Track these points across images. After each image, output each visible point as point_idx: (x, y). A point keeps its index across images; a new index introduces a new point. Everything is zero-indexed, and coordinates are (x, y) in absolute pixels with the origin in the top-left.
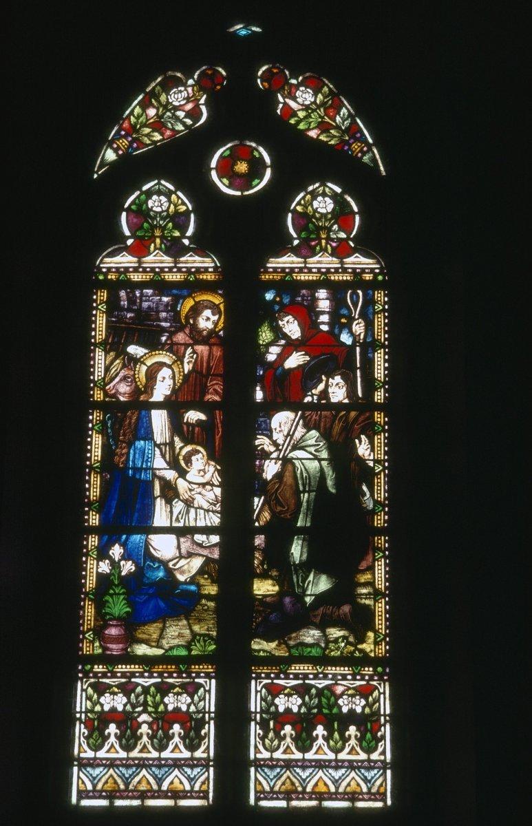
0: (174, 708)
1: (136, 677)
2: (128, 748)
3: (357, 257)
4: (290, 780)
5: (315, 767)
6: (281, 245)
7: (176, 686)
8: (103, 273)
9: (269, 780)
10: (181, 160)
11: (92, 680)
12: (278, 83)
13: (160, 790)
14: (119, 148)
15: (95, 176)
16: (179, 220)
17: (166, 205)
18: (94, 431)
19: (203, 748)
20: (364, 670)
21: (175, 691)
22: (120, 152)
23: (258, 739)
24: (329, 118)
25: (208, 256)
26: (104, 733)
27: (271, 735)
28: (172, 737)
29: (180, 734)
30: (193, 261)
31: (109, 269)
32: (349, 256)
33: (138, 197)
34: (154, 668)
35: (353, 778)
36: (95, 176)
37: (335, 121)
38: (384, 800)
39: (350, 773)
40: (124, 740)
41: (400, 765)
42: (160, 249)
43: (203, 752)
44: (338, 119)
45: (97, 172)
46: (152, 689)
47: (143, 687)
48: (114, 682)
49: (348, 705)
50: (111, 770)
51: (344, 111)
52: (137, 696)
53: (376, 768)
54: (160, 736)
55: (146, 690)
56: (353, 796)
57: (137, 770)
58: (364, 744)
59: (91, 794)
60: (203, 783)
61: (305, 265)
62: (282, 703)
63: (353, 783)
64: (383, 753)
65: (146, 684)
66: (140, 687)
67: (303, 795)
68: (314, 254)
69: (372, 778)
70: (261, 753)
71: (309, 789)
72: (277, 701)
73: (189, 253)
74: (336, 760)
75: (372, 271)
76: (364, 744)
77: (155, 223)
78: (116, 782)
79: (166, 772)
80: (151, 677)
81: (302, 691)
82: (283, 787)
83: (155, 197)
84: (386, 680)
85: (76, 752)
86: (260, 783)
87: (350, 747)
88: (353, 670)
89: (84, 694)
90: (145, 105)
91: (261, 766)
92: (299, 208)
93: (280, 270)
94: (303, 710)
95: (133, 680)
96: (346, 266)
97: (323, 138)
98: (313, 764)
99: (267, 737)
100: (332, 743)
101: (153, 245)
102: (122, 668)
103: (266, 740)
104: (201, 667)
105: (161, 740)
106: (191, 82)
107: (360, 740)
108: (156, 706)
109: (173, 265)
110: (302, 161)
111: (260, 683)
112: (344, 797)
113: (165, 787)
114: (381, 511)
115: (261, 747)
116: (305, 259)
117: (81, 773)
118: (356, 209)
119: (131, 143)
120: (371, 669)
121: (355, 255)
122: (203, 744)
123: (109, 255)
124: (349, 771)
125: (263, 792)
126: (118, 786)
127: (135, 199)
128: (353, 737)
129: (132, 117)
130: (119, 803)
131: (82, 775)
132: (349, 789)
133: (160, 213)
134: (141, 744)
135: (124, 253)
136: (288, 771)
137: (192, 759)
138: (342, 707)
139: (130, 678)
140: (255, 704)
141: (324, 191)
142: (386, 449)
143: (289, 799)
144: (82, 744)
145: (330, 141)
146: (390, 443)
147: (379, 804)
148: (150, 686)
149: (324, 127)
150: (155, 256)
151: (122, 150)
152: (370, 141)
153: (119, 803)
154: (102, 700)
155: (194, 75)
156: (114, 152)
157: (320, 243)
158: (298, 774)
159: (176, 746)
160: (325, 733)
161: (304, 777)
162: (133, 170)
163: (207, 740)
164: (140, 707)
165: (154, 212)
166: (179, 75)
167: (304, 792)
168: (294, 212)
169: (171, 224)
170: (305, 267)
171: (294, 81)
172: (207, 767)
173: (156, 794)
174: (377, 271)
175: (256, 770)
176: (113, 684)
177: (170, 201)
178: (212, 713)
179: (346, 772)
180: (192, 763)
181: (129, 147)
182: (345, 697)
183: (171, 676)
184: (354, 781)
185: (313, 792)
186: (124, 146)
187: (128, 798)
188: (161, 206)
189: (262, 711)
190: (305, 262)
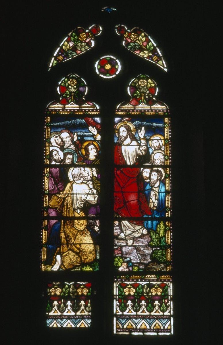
0: (128, 294)
1: (138, 281)
2: (75, 311)
3: (157, 105)
4: (131, 323)
5: (141, 318)
6: (126, 100)
7: (128, 285)
9: (163, 324)
10: (82, 66)
13: (136, 329)
15: (166, 70)
16: (152, 90)
19: (168, 311)
23: (117, 307)
24: (144, 46)
25: (164, 105)
26: (126, 304)
30: (158, 107)
31: (52, 110)
32: (84, 104)
34: (131, 277)
35: (69, 323)
36: (166, 70)
38: (170, 332)
39: (142, 320)
40: (162, 308)
41: (177, 316)
42: (144, 102)
43: (169, 313)
46: (146, 286)
47: (142, 285)
48: (129, 283)
50: (69, 320)
51: (150, 44)
52: (66, 289)
53: (65, 318)
56: (144, 330)
59: (163, 330)
62: (126, 291)
63: (130, 324)
64: (170, 312)
65: (143, 284)
67: (136, 330)
69: (151, 322)
70: (119, 312)
71: (138, 328)
72: (78, 291)
74: (150, 315)
75: (163, 110)
76: (162, 308)
77: (141, 91)
79: (51, 321)
81: (135, 286)
82: (128, 327)
87: (54, 310)
89: (117, 288)
90: (68, 41)
92: (62, 84)
93: (54, 110)
94: (62, 294)
95: (137, 282)
96: (152, 109)
98: (140, 317)
100: (87, 308)
102: (163, 277)
103: (148, 307)
105: (123, 308)
107: (133, 306)
108: (147, 293)
110: (135, 67)
113: (125, 327)
114: (168, 211)
123: (51, 104)
124: (142, 319)
125: (119, 328)
126: (160, 327)
127: (133, 81)
128: (83, 306)
129: (63, 46)
130: (160, 334)
134: (128, 309)
135: (157, 104)
136: (82, 321)
140: (116, 292)
143: (157, 332)
144: (117, 309)
147: (168, 334)
148: (144, 285)
150: (71, 104)
152: (161, 55)
153: (160, 334)
157: (141, 99)
159: (130, 310)
161: (136, 322)
162: (63, 69)
165: (141, 86)
167: (150, 328)
168: (60, 86)
173: (133, 330)
174: (165, 111)
176: (129, 284)
178: (171, 296)
179: (66, 320)
180: (163, 317)
184: (130, 324)
186: (156, 58)
189: (119, 295)
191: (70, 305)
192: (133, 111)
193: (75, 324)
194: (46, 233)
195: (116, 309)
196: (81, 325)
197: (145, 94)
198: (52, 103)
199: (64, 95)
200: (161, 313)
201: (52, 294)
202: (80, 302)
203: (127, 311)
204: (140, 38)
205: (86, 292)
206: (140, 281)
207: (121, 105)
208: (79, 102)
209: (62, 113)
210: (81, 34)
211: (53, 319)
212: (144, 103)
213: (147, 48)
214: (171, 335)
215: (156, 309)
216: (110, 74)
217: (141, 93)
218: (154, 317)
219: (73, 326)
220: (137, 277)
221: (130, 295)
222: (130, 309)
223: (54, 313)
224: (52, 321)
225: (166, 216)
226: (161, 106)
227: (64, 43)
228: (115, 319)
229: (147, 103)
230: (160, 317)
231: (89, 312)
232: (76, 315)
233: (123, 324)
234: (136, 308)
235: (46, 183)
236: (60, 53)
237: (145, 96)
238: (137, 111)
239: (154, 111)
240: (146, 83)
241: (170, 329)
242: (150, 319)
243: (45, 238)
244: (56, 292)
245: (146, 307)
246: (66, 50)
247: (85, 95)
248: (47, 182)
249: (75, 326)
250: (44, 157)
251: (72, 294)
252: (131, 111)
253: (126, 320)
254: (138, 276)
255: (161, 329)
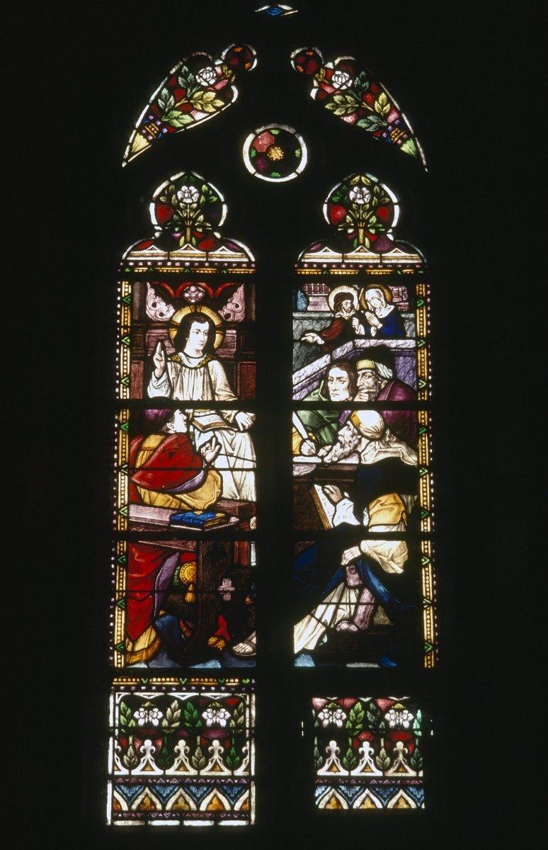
0: (145, 723)
1: (172, 691)
3: (223, 250)
6: (143, 235)
8: (130, 267)
9: (383, 801)
10: (207, 152)
11: (124, 694)
12: (312, 66)
13: (198, 811)
14: (401, 138)
15: (124, 165)
17: (196, 196)
18: (121, 432)
19: (243, 766)
20: (229, 682)
21: (147, 705)
22: (151, 138)
25: (415, 252)
27: (198, 751)
28: (329, 755)
29: (370, 752)
30: (397, 256)
31: (136, 263)
33: (167, 188)
36: (124, 165)
37: (373, 107)
38: (249, 819)
44: (377, 105)
45: (126, 160)
47: (178, 700)
49: (328, 719)
54: (383, 755)
55: (182, 705)
57: (208, 789)
58: (228, 760)
60: (245, 802)
61: (169, 258)
64: (248, 769)
65: (183, 699)
66: (176, 701)
68: (352, 249)
70: (119, 770)
72: (204, 715)
73: (220, 247)
77: (185, 215)
78: (338, 802)
80: (189, 690)
82: (176, 805)
83: (184, 188)
84: (253, 692)
85: (110, 771)
86: (118, 802)
88: (218, 681)
89: (117, 709)
91: (119, 785)
97: (362, 124)
99: (194, 755)
101: (356, 241)
102: (170, 681)
104: (120, 680)
105: (349, 759)
106: (218, 62)
107: (340, 755)
109: (379, 262)
110: (345, 151)
111: (119, 695)
112: (171, 816)
113: (203, 808)
115: (119, 764)
116: (207, 252)
117: (115, 792)
118: (395, 200)
119: (161, 127)
120: (237, 680)
121: (395, 250)
122: (244, 762)
124: (177, 788)
125: (121, 811)
126: (409, 805)
127: (164, 190)
129: (159, 101)
131: (116, 794)
132: (211, 807)
133: (363, 205)
135: (326, 248)
137: (198, 777)
138: (322, 721)
139: (166, 692)
140: (114, 718)
141: (189, 179)
142: (431, 451)
143: (181, 819)
144: (116, 761)
145: (368, 128)
146: (435, 444)
147: (243, 823)
149: (361, 113)
150: (185, 249)
151: (152, 136)
153: (187, 823)
154: (136, 715)
155: (336, 58)
156: (144, 138)
158: (412, 793)
159: (148, 764)
160: (372, 750)
163: (248, 757)
164: (177, 722)
166: (203, 54)
167: (164, 810)
169: (202, 216)
170: (381, 263)
171: (330, 65)
172: (248, 787)
175: (114, 789)
177: (200, 192)
181: (158, 132)
182: (391, 711)
183: (208, 690)
184: (215, 799)
185: (172, 811)
187: (163, 818)
188: (191, 198)
190: (381, 258)
191: (336, 752)
192: (164, 263)
193: (350, 800)
194: (424, 577)
195: (114, 765)
196: (397, 803)
197: (366, 225)
198: (140, 243)
199: (340, 228)
200: (193, 772)
201: (326, 722)
202: (362, 746)
203: (176, 765)
204: (183, 82)
205: (156, 718)
206: (174, 692)
207: (133, 250)
208: (206, 243)
209: (336, 273)
210: (202, 70)
211: (327, 785)
212: (192, 245)
213: (375, 111)
214: (248, 827)
215: (365, 763)
216: (280, 173)
217: (356, 221)
218: (208, 781)
219: (379, 806)
220: (159, 680)
221: (149, 725)
222: (367, 764)
223: (143, 770)
224: (325, 793)
225: (422, 530)
226: (403, 254)
227: (160, 92)
228: (110, 786)
229: (373, 248)
230: (203, 781)
231: (416, 769)
232: (384, 778)
233: (164, 798)
234: (383, 759)
235: (124, 447)
236: (151, 117)
237: (193, 228)
238: (348, 266)
239: (178, 264)
240: (367, 196)
241: (249, 812)
242: (349, 786)
243: (121, 581)
244: (334, 720)
245: (223, 756)
246: (166, 110)
247: (393, 228)
248: (124, 443)
249: (383, 805)
250: (117, 382)
251: (191, 723)
252: (160, 264)
253: (171, 788)
254: (122, 679)
255: (224, 811)
